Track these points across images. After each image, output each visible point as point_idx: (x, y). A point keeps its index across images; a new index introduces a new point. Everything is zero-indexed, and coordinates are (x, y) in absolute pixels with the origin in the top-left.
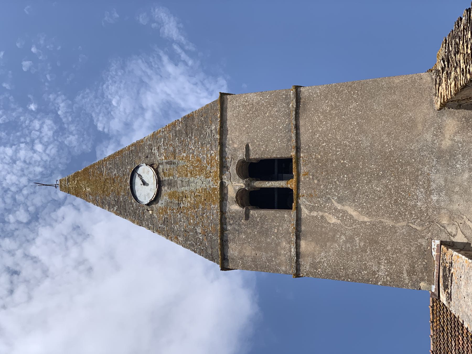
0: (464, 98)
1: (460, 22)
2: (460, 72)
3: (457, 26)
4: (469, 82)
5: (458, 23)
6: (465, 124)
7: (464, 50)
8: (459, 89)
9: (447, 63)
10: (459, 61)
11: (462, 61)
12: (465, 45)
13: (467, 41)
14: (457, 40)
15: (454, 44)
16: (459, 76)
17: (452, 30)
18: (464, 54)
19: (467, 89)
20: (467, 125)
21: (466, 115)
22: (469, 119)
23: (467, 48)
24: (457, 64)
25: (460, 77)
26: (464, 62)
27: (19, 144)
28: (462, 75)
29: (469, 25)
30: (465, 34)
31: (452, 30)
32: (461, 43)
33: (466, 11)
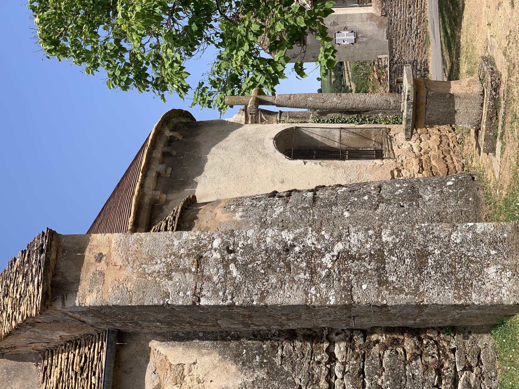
0: (8, 347)
1: (13, 262)
2: (6, 317)
3: (10, 267)
4: (14, 330)
5: (12, 264)
6: (5, 377)
7: (13, 294)
8: (2, 337)
9: (379, 306)
10: (7, 305)
11: (10, 306)
12: (15, 288)
13: (17, 285)
14: (8, 282)
15: (5, 286)
16: (4, 322)
17: (5, 270)
18: (13, 298)
19: (12, 338)
20: (8, 377)
21: (8, 366)
22: (11, 371)
23: (17, 292)
24: (4, 308)
25: (5, 323)
26: (12, 307)
27: (99, 336)
28: (8, 321)
29: (22, 268)
30: (17, 276)
31: (5, 270)
32: (12, 285)
33: (21, 253)
